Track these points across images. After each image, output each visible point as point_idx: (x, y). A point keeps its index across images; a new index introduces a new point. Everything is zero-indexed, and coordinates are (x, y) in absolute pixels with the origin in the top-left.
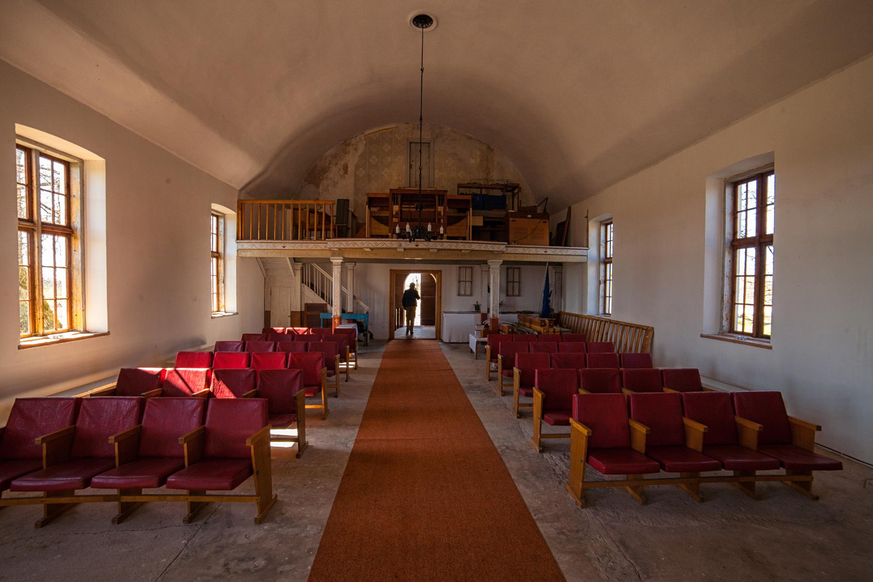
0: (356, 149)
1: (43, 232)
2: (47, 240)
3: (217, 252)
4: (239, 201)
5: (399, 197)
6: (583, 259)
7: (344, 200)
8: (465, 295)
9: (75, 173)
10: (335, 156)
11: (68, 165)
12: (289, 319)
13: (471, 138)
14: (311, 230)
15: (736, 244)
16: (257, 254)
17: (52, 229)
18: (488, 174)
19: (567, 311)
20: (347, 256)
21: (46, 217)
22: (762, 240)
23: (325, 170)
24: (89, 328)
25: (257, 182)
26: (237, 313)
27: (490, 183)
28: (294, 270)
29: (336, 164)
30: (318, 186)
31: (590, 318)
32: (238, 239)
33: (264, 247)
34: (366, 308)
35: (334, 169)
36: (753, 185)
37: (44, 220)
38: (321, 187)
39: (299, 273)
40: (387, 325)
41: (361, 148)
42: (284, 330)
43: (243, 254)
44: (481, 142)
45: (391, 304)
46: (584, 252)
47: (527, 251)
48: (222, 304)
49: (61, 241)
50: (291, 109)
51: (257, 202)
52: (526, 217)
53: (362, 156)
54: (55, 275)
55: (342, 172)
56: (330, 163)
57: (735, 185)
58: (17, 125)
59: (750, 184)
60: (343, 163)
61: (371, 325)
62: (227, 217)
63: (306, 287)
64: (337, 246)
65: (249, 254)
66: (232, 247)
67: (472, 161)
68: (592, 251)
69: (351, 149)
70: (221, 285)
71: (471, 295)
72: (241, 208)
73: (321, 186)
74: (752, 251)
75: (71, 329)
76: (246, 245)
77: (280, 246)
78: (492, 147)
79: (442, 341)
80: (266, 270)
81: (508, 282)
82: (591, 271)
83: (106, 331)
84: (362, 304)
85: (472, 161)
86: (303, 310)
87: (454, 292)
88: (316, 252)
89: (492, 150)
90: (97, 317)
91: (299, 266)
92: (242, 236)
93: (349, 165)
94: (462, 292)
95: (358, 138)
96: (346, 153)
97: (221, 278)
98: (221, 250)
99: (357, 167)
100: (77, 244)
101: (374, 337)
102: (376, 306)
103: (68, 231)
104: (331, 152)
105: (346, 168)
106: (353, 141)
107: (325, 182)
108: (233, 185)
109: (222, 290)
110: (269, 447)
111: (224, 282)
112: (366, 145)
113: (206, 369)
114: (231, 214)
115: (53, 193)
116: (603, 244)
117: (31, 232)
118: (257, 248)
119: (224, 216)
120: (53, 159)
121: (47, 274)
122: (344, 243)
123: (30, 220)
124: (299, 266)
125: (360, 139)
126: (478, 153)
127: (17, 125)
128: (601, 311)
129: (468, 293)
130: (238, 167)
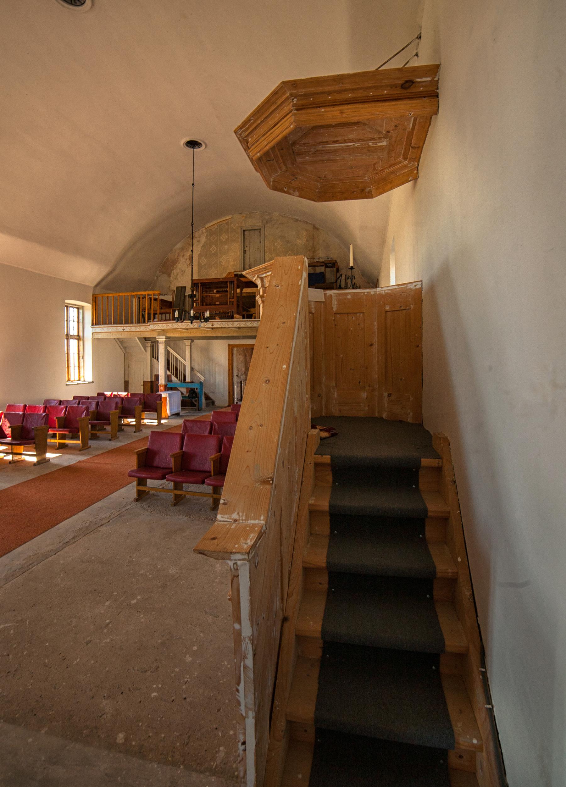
0: (199, 241)
3: (78, 336)
4: (93, 295)
5: (200, 285)
7: (182, 287)
9: (81, 311)
10: (182, 249)
12: (142, 387)
13: (297, 220)
14: (155, 314)
16: (116, 337)
18: (314, 252)
20: (168, 335)
23: (175, 262)
25: (110, 278)
26: (93, 382)
27: (316, 260)
28: (145, 347)
29: (184, 255)
30: (169, 275)
32: (93, 324)
35: (182, 260)
38: (172, 276)
39: (149, 349)
40: (227, 394)
41: (203, 240)
42: (112, 394)
43: (96, 336)
44: (307, 223)
48: (82, 375)
50: (121, 225)
51: (111, 295)
53: (203, 246)
56: (179, 255)
61: (213, 393)
62: (85, 309)
65: (100, 336)
66: (89, 331)
67: (299, 242)
70: (81, 360)
72: (95, 301)
73: (172, 275)
76: (98, 329)
77: (120, 329)
78: (317, 226)
80: (125, 348)
84: (199, 375)
85: (299, 242)
86: (153, 380)
88: (146, 333)
89: (317, 229)
92: (96, 322)
95: (200, 232)
97: (81, 355)
98: (81, 334)
99: (200, 256)
102: (217, 377)
104: (179, 245)
107: (175, 272)
108: (87, 284)
109: (81, 364)
110: (36, 451)
111: (83, 358)
112: (207, 237)
114: (88, 307)
118: (107, 331)
119: (83, 307)
122: (170, 325)
124: (149, 344)
125: (203, 233)
126: (305, 233)
130: (89, 272)
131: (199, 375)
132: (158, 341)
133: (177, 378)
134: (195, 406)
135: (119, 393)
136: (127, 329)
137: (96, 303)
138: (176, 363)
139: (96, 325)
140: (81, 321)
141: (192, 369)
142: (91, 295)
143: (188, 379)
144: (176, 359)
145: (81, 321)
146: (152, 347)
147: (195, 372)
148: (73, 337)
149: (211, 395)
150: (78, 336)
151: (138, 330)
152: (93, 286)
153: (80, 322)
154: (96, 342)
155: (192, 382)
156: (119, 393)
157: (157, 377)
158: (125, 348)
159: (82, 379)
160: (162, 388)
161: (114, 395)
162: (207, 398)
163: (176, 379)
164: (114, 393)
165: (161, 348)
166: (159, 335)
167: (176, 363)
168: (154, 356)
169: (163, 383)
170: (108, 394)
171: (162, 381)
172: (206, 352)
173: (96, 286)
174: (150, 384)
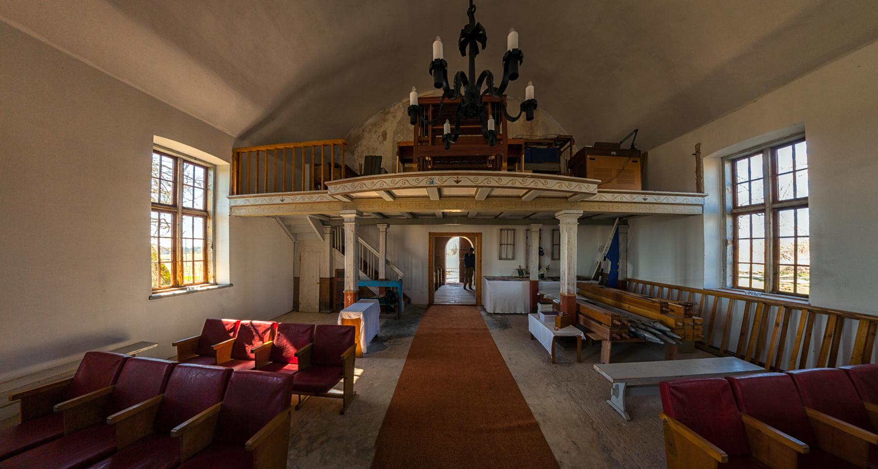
0: (394, 117)
1: (183, 214)
2: (187, 220)
3: (206, 210)
4: (233, 150)
6: (697, 210)
8: (506, 259)
9: (211, 173)
10: (375, 125)
11: (207, 169)
15: (736, 212)
17: (192, 212)
19: (642, 277)
20: (361, 209)
21: (187, 204)
22: (735, 211)
24: (218, 281)
26: (231, 285)
28: (322, 234)
30: (353, 153)
31: (706, 292)
32: (232, 193)
33: (259, 202)
34: (401, 274)
36: (757, 161)
37: (185, 205)
39: (328, 237)
42: (236, 324)
43: (237, 212)
45: (430, 268)
46: (699, 200)
47: (618, 198)
48: (211, 274)
49: (199, 221)
52: (610, 155)
53: (400, 122)
54: (159, 243)
55: (381, 139)
57: (733, 162)
58: (155, 137)
59: (753, 159)
60: (382, 130)
61: (409, 289)
63: (337, 251)
64: (340, 191)
65: (243, 212)
68: (711, 198)
69: (390, 117)
71: (513, 259)
72: (237, 159)
74: (759, 219)
75: (206, 281)
76: (240, 201)
77: (277, 200)
79: (485, 310)
80: (295, 235)
81: (553, 245)
82: (710, 227)
83: (228, 283)
84: (396, 270)
87: (495, 255)
90: (223, 274)
91: (328, 229)
93: (388, 131)
94: (504, 256)
95: (396, 107)
96: (384, 120)
98: (210, 208)
99: (395, 133)
100: (210, 223)
101: (412, 302)
102: (414, 270)
103: (205, 214)
105: (384, 135)
106: (392, 109)
113: (270, 323)
114: (224, 166)
115: (194, 187)
116: (729, 188)
117: (175, 215)
119: (215, 167)
120: (195, 164)
121: (187, 244)
123: (175, 205)
124: (328, 229)
127: (155, 137)
128: (729, 283)
129: (510, 257)
131: (396, 270)
132: (343, 220)
133: (365, 272)
134: (393, 310)
135: (255, 322)
136: (288, 199)
137: (238, 161)
138: (365, 256)
139: (237, 194)
140: (211, 187)
141: (387, 262)
142: (231, 149)
143: (382, 276)
144: (365, 249)
145: (211, 187)
146: (333, 234)
147: (392, 266)
148: (192, 212)
149: (409, 295)
150: (206, 210)
151: (307, 200)
152: (235, 136)
153: (209, 189)
154: (238, 223)
155: (386, 279)
156: (255, 322)
157: (341, 273)
158: (295, 235)
159: (211, 281)
160: (349, 298)
161: (243, 325)
162: (405, 296)
163: (364, 275)
164: (243, 322)
165: (349, 230)
166: (345, 206)
167: (365, 256)
168: (338, 246)
169: (352, 289)
170: (229, 321)
171: (350, 285)
172: (401, 241)
173: (244, 136)
174: (328, 282)
